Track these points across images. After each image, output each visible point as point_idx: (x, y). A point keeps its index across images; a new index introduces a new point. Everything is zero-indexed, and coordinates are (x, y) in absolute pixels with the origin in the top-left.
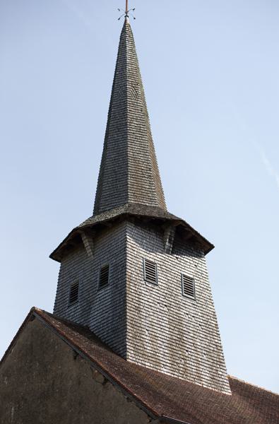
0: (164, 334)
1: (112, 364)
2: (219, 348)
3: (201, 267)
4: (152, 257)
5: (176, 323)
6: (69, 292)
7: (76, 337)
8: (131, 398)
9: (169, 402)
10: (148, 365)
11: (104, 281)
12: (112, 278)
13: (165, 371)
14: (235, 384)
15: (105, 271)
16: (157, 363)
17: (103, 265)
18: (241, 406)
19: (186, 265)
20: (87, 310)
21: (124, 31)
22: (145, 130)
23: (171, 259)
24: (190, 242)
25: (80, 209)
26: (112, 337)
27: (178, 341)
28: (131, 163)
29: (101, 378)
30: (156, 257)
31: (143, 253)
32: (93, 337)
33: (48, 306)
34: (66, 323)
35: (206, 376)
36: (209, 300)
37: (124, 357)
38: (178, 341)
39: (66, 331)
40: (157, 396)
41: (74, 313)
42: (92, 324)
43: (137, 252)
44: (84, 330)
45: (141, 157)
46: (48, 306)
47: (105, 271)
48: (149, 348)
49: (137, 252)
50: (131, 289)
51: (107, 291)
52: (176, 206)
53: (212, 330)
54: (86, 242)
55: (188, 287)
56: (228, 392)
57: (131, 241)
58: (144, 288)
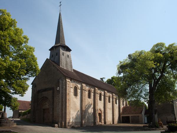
0: (65, 63)
1: (58, 68)
2: (72, 65)
3: (70, 53)
4: (63, 52)
5: (66, 61)
6: (51, 56)
7: (53, 63)
8: (61, 73)
9: (66, 73)
10: (63, 67)
11: (57, 55)
12: (58, 54)
13: (65, 68)
14: (74, 70)
15: (57, 53)
16: (64, 67)
17: (57, 52)
18: (75, 74)
19: (68, 53)
20: (54, 59)
21: (60, 14)
22: (62, 26)
23: (66, 52)
24: (68, 49)
25: (53, 44)
26: (58, 63)
27: (66, 64)
28: (60, 37)
29: (57, 70)
30: (64, 52)
31: (62, 51)
32: (55, 63)
33: (105, 80)
34: (52, 61)
35: (70, 69)
36: (71, 58)
37: (60, 66)
38: (66, 64)
39: (52, 62)
40: (64, 72)
41: (52, 59)
42: (55, 61)
43: (62, 51)
44: (54, 62)
45: (62, 36)
46: (105, 80)
47: (57, 53)
48: (63, 65)
49: (62, 51)
50: (61, 56)
51: (57, 56)
52: (67, 44)
53: (71, 63)
54: (54, 48)
55: (68, 56)
56: (73, 71)
57: (61, 49)
58: (62, 56)
